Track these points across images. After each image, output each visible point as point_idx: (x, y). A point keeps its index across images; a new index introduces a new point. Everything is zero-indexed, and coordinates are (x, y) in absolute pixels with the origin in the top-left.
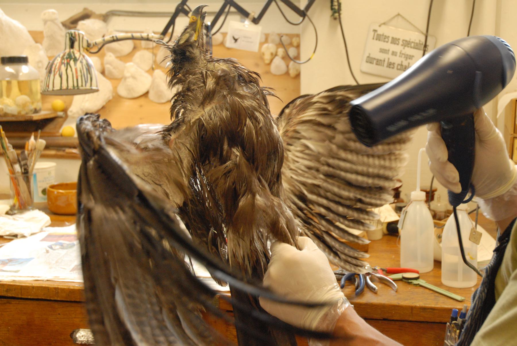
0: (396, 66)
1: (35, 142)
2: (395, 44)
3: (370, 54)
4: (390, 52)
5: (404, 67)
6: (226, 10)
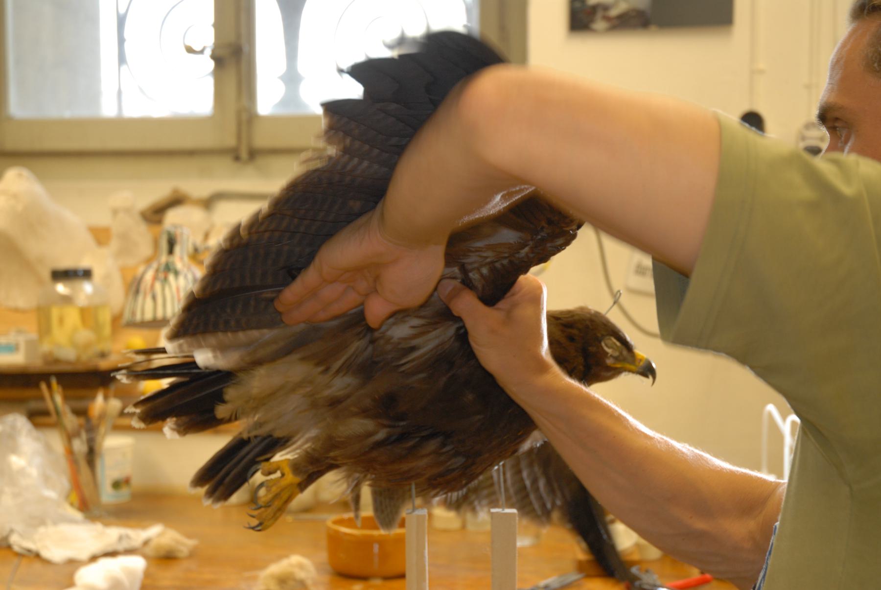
1: (101, 403)
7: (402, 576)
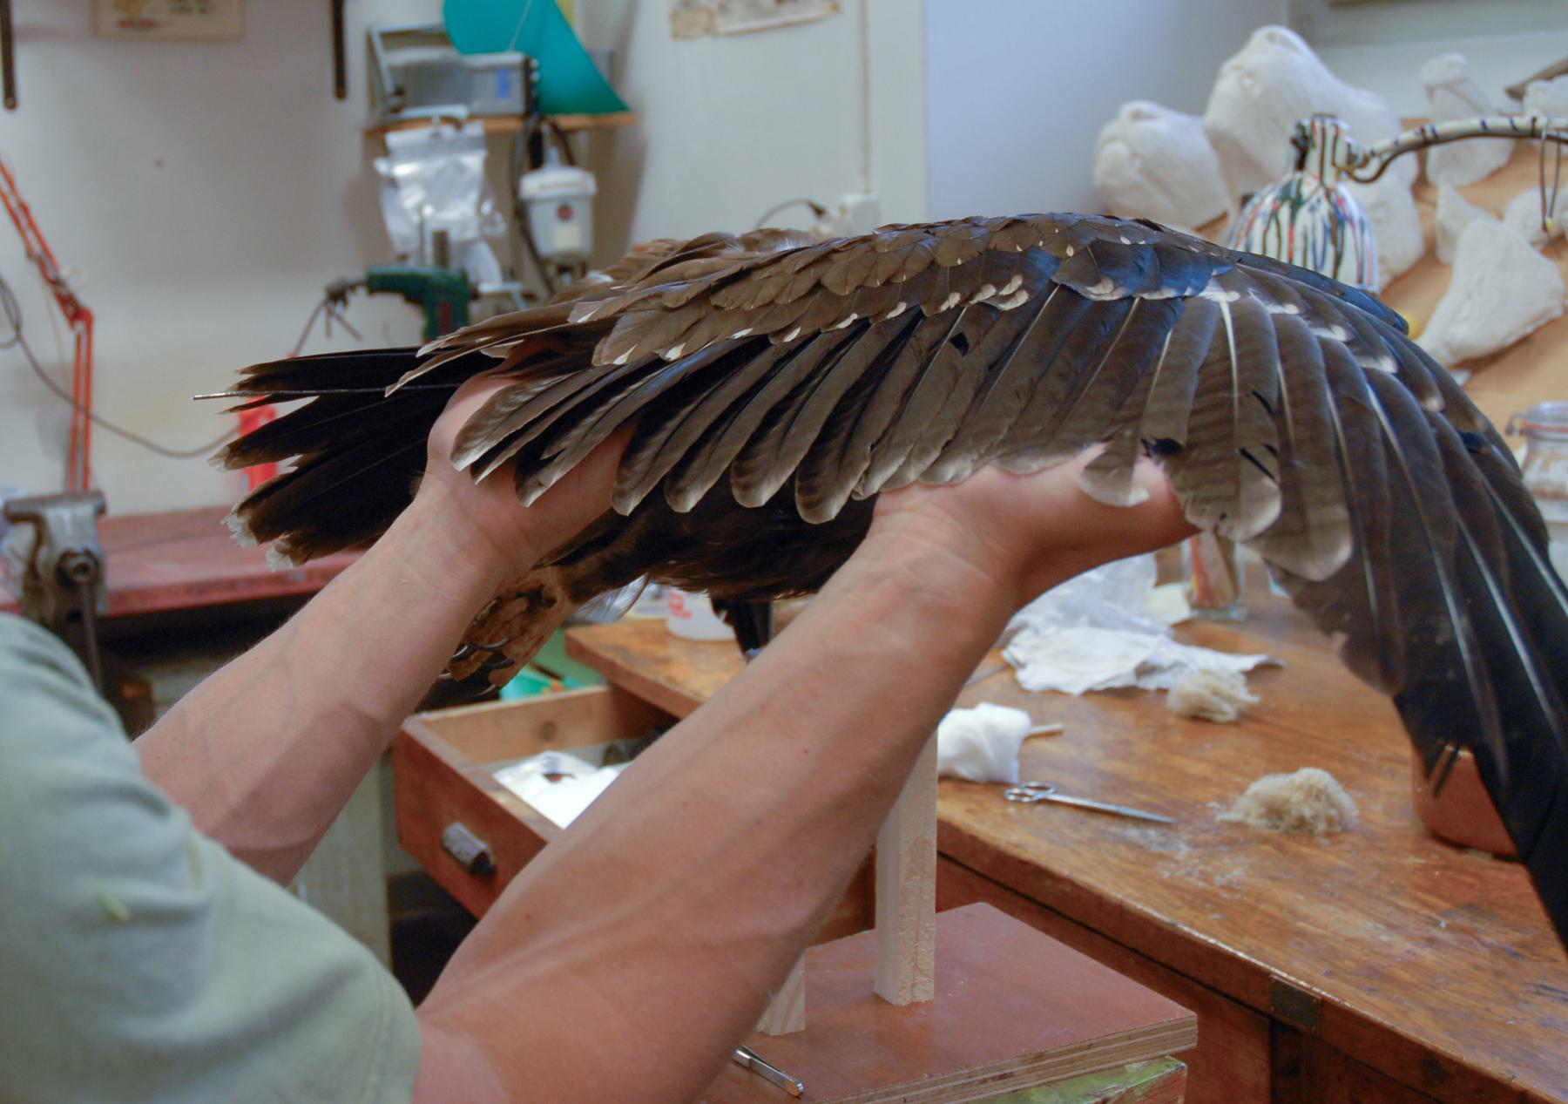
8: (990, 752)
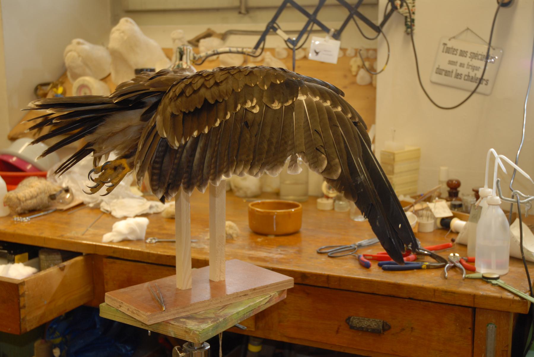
0: (463, 76)
2: (463, 56)
3: (439, 66)
4: (458, 64)
5: (471, 78)
6: (309, 28)
7: (295, 233)
8: (138, 231)
